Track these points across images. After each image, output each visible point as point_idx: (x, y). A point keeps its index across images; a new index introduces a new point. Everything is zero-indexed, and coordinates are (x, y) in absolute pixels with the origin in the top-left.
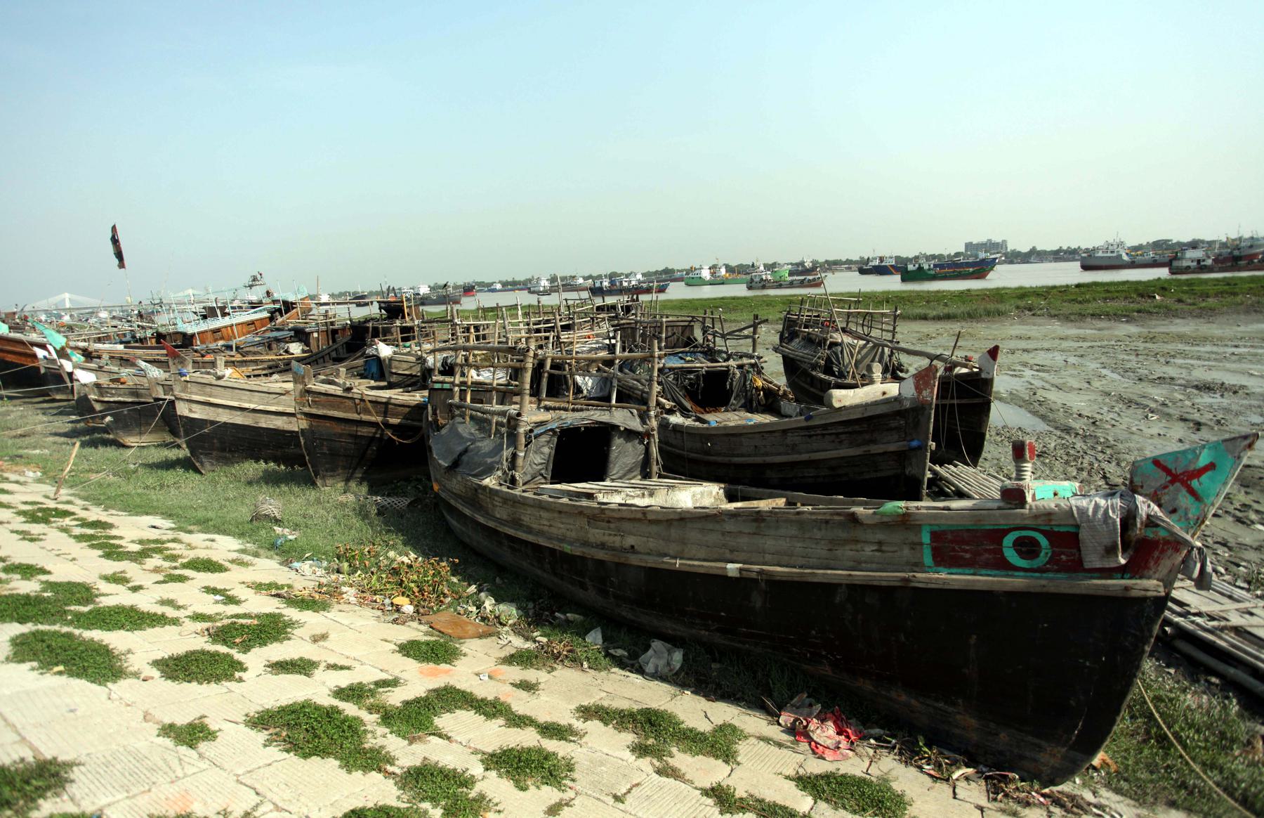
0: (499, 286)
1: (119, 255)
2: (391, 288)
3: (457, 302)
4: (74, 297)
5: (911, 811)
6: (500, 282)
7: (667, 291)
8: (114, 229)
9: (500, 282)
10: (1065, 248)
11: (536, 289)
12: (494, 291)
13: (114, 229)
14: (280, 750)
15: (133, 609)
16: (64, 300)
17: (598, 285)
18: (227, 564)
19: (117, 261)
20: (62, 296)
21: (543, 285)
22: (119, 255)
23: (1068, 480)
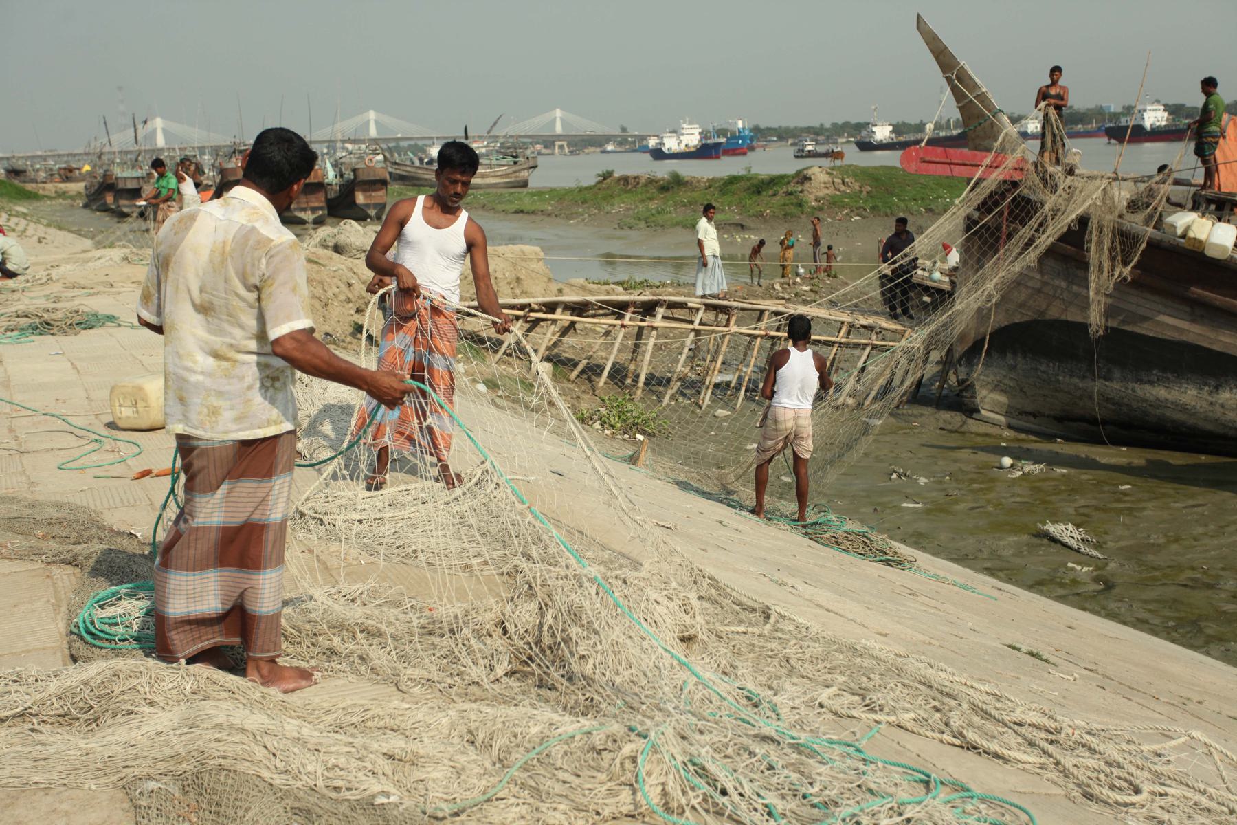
4: (387, 120)
20: (357, 120)
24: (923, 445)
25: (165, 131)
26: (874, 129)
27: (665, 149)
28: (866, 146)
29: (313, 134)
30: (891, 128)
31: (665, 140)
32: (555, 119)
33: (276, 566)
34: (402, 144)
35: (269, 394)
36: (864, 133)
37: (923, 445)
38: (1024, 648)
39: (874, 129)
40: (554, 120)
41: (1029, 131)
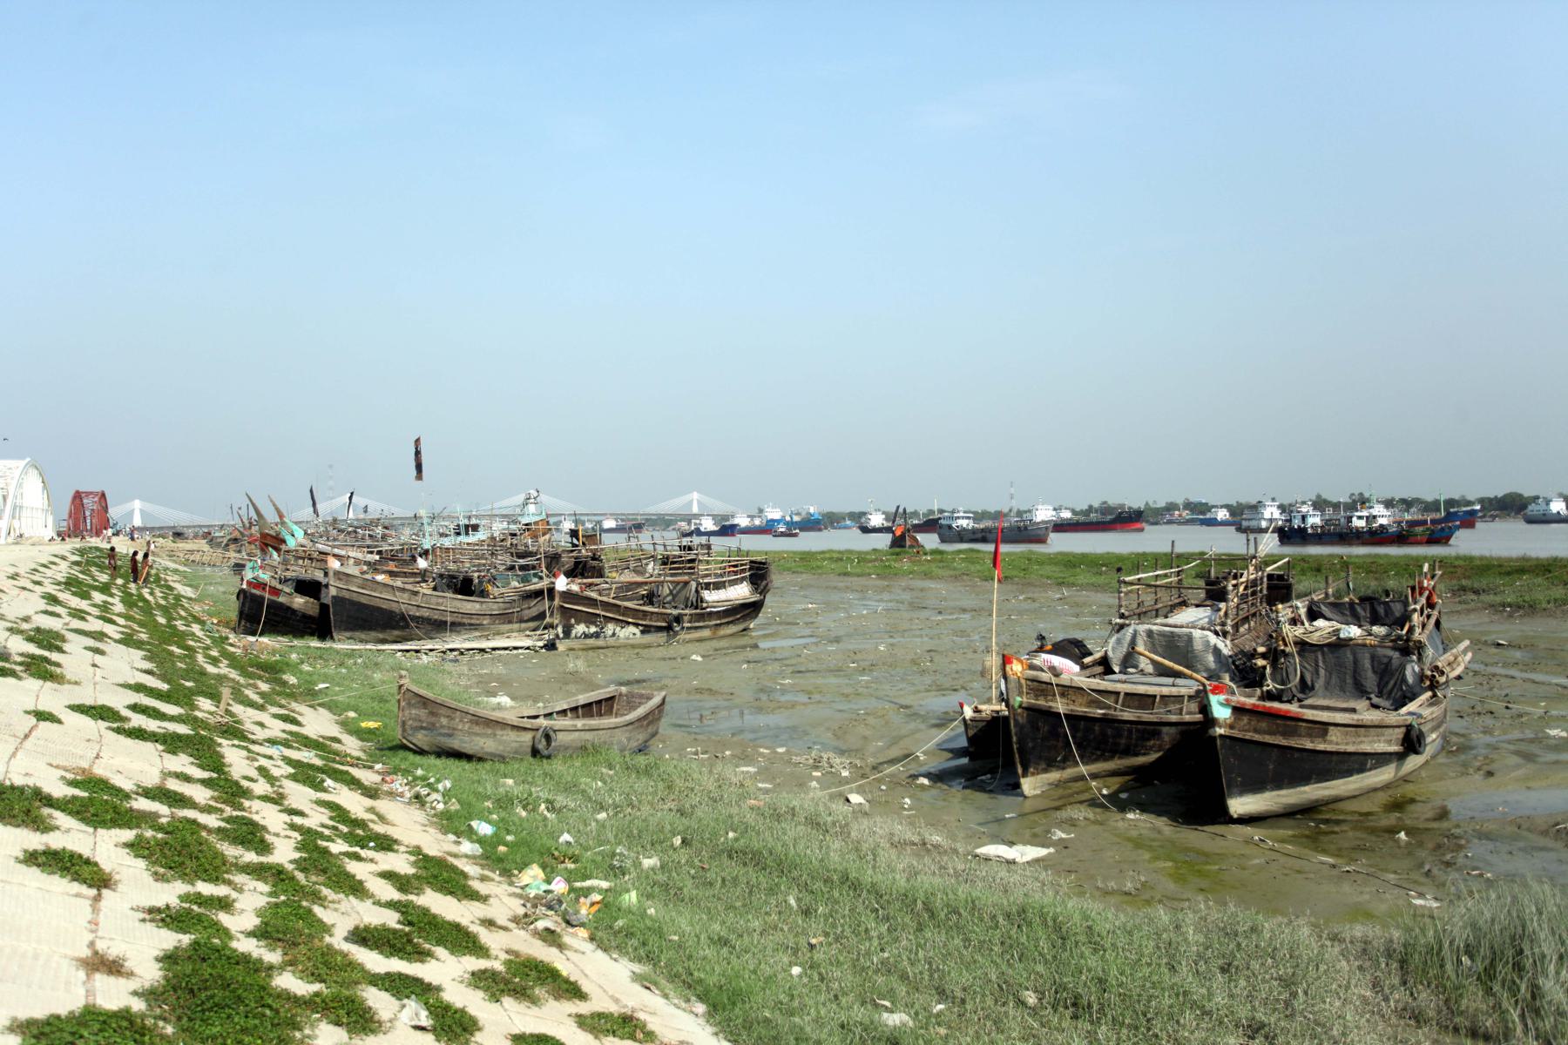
0: (1222, 514)
1: (419, 467)
2: (901, 510)
3: (1041, 540)
4: (149, 507)
5: (478, 1037)
6: (1227, 507)
7: (1452, 541)
8: (417, 441)
9: (1227, 507)
10: (1096, 505)
11: (1253, 524)
12: (1212, 523)
13: (417, 441)
14: (63, 778)
15: (182, 795)
16: (131, 513)
17: (1296, 523)
18: (512, 925)
19: (414, 473)
20: (687, 498)
21: (1267, 515)
22: (419, 467)
23: (577, 682)
24: (76, 683)
25: (699, 502)
26: (870, 517)
27: (703, 530)
28: (865, 530)
29: (918, 510)
30: (884, 516)
31: (703, 522)
32: (133, 511)
33: (79, 820)
34: (395, 522)
35: (33, 671)
36: (863, 520)
37: (76, 683)
38: (610, 993)
39: (870, 517)
40: (692, 501)
41: (1219, 519)
